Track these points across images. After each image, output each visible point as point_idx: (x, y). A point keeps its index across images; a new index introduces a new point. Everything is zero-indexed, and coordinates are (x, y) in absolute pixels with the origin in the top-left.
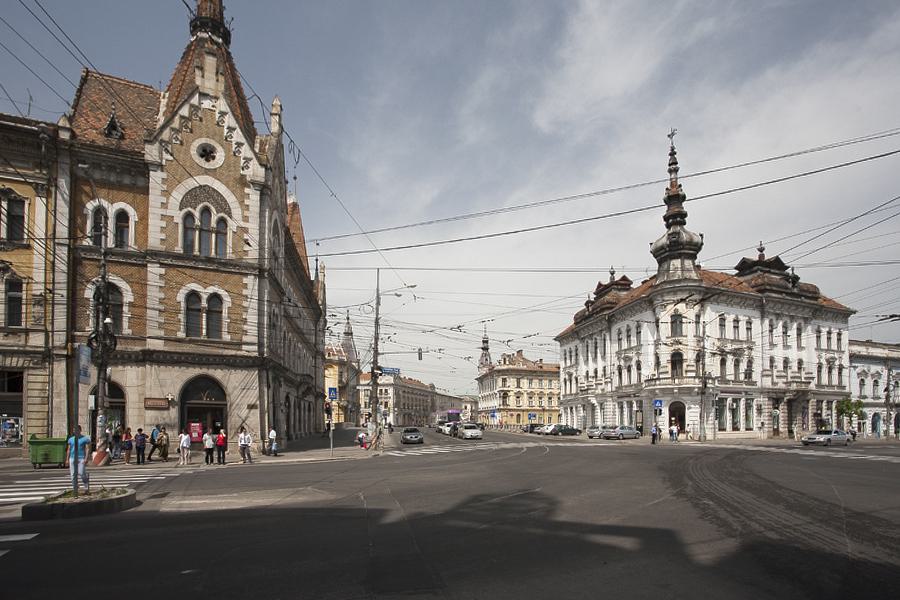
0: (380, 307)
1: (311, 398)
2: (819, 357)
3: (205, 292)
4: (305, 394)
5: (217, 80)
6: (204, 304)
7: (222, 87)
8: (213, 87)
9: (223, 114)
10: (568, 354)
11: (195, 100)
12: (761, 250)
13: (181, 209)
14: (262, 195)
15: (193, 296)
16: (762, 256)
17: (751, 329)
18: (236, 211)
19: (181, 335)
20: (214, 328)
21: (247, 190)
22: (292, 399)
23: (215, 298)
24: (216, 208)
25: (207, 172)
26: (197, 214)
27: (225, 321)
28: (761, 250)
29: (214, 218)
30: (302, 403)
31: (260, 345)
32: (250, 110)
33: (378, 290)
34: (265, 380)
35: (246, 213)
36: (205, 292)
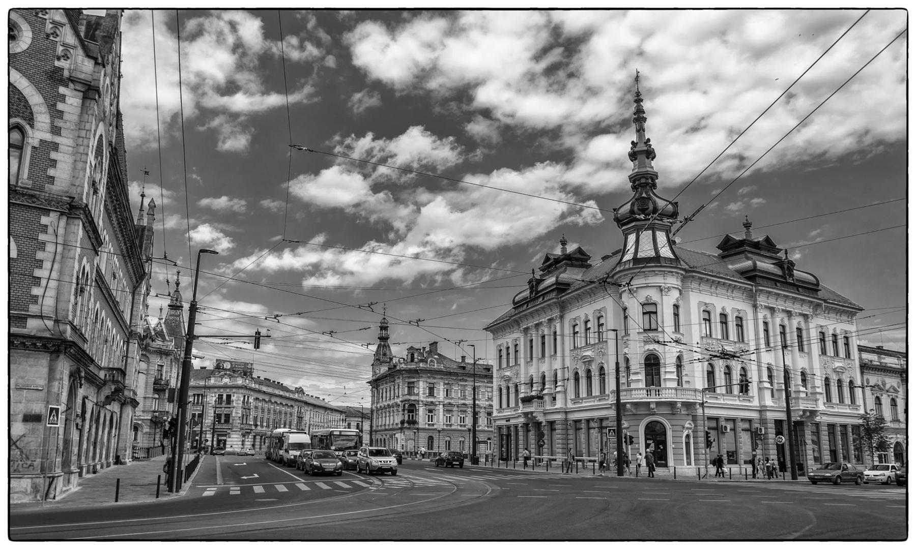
21: (62, 90)
22: (89, 406)
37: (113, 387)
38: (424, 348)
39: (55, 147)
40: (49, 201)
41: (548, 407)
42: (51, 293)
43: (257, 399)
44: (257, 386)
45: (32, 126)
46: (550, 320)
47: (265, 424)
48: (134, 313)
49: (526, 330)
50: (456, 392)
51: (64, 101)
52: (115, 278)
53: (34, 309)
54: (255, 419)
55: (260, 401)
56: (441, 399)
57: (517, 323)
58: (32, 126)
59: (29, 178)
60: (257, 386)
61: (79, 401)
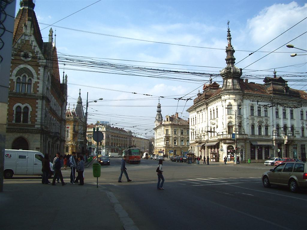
0: (88, 108)
1: (59, 142)
2: (303, 123)
3: (23, 106)
4: (56, 141)
5: (31, 30)
6: (22, 111)
7: (32, 32)
8: (29, 32)
9: (32, 41)
10: (212, 112)
11: (23, 38)
12: (275, 73)
13: (16, 77)
14: (44, 68)
15: (19, 107)
16: (275, 76)
17: (267, 111)
18: (35, 75)
19: (14, 122)
20: (25, 120)
21: (39, 68)
22: (50, 143)
23: (26, 108)
24: (28, 75)
25: (25, 63)
26: (21, 78)
27: (30, 116)
28: (275, 73)
29: (27, 79)
30: (54, 145)
31: (41, 125)
32: (41, 33)
33: (87, 100)
34: (43, 138)
35: (39, 76)
36: (23, 106)
37: (56, 138)
38: (174, 115)
39: (38, 83)
40: (38, 96)
41: (274, 132)
42: (41, 106)
43: (112, 136)
44: (112, 131)
45: (33, 78)
46: (204, 109)
47: (113, 145)
48: (62, 113)
49: (198, 112)
50: (185, 132)
51: (40, 71)
52: (55, 105)
53: (36, 123)
54: (112, 143)
55: (116, 137)
56: (179, 136)
57: (195, 109)
58: (33, 78)
59: (33, 91)
60: (112, 131)
61: (48, 143)
